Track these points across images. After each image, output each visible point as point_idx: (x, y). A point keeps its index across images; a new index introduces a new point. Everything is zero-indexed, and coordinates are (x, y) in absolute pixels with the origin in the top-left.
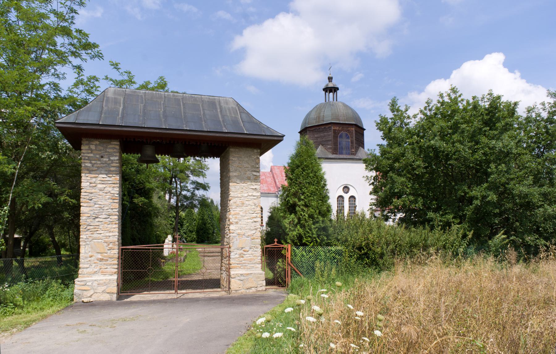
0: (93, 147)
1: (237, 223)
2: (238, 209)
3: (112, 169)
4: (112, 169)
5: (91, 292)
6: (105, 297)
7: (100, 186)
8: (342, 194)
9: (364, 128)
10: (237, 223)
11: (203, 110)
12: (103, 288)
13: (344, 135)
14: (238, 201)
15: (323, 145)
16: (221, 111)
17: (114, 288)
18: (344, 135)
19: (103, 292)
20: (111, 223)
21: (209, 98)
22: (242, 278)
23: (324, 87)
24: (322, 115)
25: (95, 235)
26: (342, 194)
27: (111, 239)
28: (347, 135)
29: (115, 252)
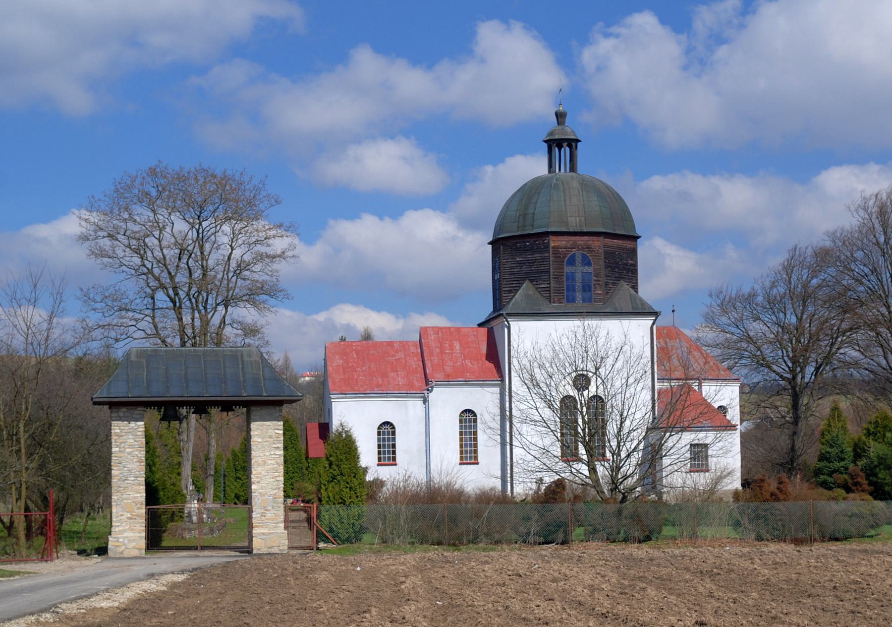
0: (121, 414)
1: (258, 482)
2: (260, 468)
3: (139, 433)
4: (139, 433)
5: (123, 548)
6: (135, 553)
7: (128, 450)
8: (573, 392)
9: (639, 232)
10: (258, 482)
11: (225, 367)
12: (134, 544)
13: (579, 259)
14: (260, 460)
15: (531, 281)
16: (243, 368)
17: (143, 543)
18: (579, 259)
19: (134, 548)
20: (139, 484)
21: (231, 351)
22: (264, 537)
23: (544, 137)
24: (531, 211)
25: (125, 496)
26: (573, 392)
27: (139, 499)
28: (584, 257)
29: (143, 511)
